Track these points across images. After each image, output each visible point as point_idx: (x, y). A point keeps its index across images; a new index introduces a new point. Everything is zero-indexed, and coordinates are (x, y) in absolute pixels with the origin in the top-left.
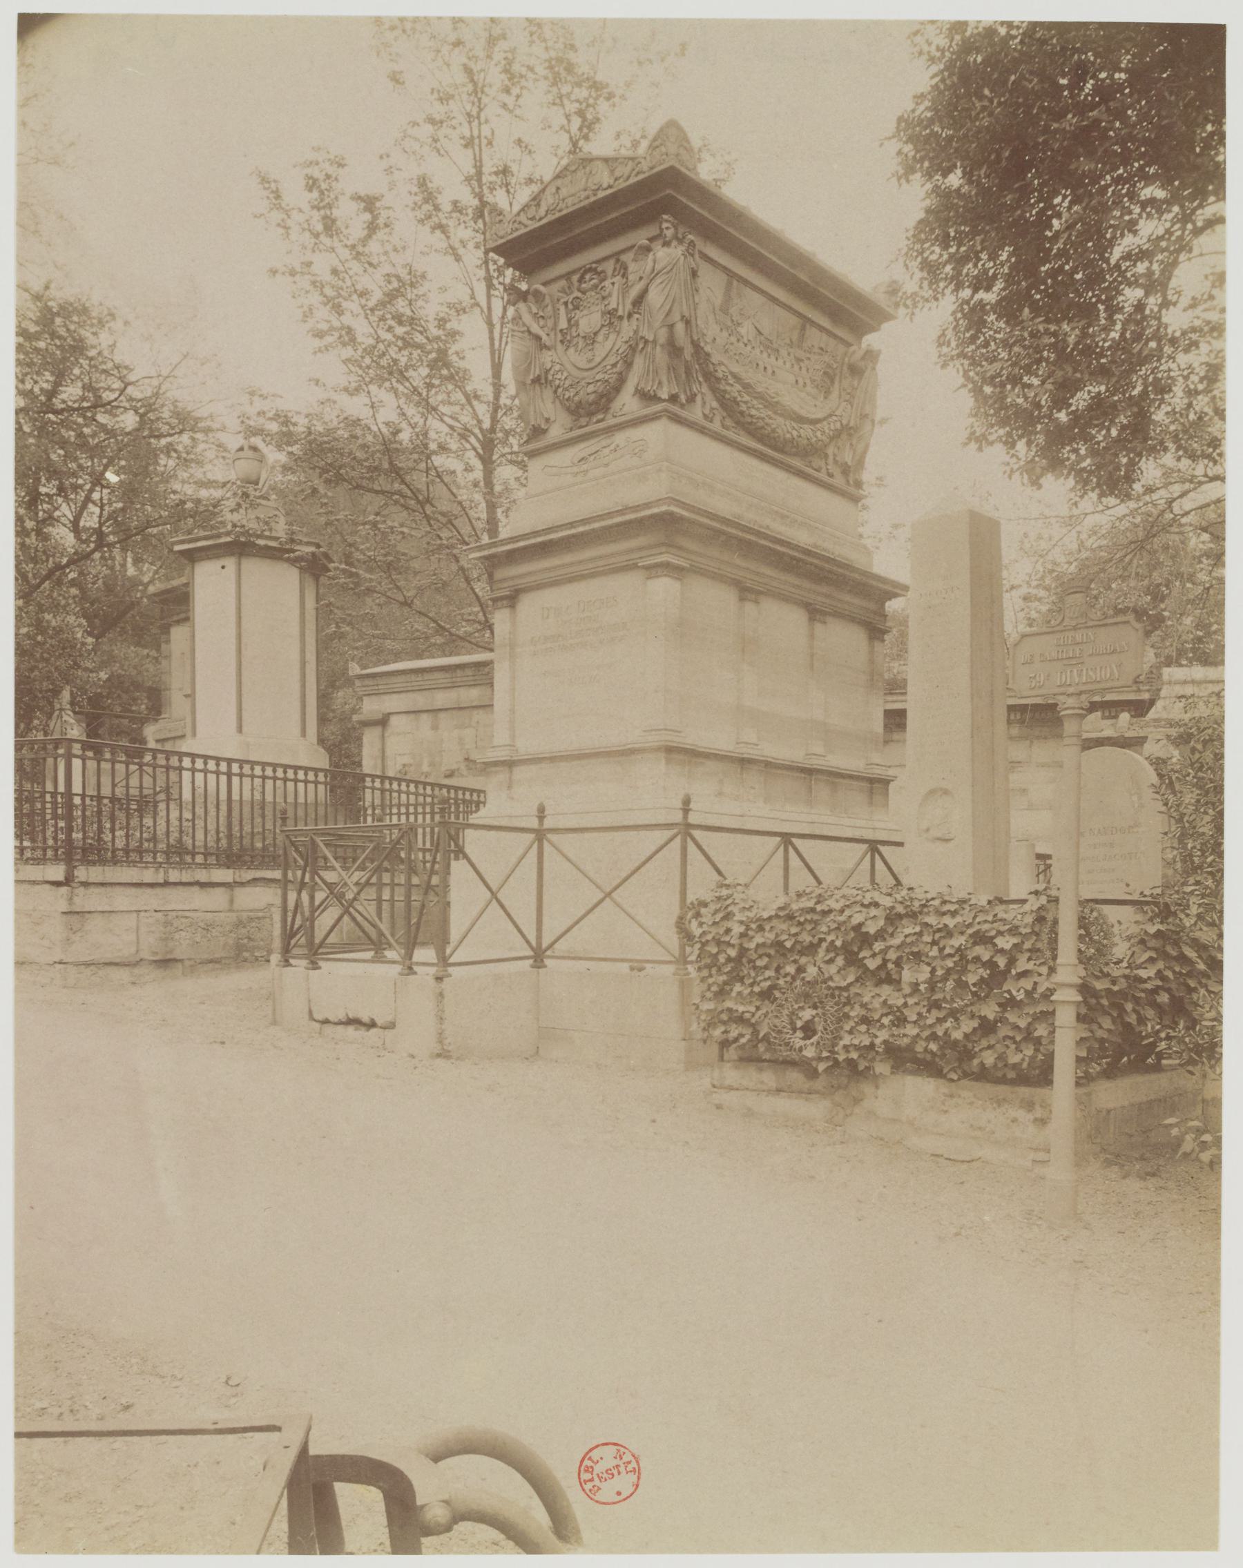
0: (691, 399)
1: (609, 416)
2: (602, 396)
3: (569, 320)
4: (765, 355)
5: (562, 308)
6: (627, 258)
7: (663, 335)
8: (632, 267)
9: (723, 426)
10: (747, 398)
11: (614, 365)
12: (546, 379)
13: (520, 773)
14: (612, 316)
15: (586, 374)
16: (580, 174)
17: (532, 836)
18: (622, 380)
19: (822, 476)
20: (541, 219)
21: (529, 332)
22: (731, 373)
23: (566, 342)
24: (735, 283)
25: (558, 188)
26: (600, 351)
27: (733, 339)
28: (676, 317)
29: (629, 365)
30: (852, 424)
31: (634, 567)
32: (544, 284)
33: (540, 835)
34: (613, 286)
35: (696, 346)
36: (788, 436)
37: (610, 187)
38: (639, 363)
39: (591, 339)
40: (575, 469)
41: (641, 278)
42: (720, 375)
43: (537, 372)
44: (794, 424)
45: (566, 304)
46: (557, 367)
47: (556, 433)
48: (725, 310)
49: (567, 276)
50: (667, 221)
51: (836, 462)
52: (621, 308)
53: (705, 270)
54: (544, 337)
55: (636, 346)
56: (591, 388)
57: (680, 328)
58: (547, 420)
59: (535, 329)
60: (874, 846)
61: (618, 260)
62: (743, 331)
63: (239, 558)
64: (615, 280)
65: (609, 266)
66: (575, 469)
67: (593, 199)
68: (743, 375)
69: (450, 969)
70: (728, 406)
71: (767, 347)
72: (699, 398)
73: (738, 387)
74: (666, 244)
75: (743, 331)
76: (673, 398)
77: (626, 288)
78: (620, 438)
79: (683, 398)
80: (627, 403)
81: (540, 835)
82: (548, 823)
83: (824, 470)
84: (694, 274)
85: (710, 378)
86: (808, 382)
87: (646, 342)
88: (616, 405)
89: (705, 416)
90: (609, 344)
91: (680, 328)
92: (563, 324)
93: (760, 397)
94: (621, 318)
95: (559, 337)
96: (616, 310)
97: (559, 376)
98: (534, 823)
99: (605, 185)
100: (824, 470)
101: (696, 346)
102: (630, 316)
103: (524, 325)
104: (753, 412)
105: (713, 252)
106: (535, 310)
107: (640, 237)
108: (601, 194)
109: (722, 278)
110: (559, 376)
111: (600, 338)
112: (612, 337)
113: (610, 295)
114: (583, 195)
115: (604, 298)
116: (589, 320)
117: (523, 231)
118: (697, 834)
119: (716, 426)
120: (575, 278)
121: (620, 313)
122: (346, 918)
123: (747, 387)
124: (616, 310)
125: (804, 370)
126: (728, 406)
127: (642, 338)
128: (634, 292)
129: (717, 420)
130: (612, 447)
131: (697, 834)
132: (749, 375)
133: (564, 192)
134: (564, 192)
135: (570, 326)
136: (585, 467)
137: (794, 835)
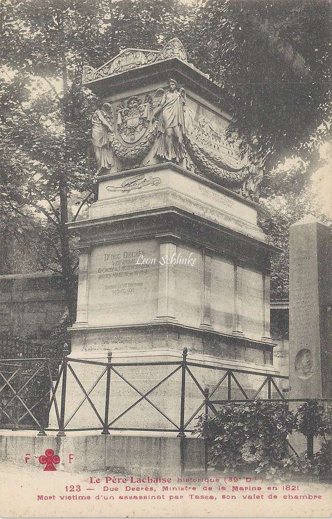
0: (181, 160)
1: (141, 166)
2: (138, 156)
3: (122, 120)
4: (215, 140)
5: (119, 114)
6: (153, 95)
7: (170, 131)
8: (155, 99)
9: (195, 172)
10: (206, 160)
11: (145, 143)
12: (110, 146)
13: (91, 337)
14: (144, 121)
15: (131, 146)
16: (131, 56)
17: (105, 367)
18: (149, 149)
19: (240, 195)
20: (110, 75)
21: (102, 123)
22: (199, 148)
23: (120, 129)
24: (201, 107)
25: (119, 61)
26: (137, 136)
27: (200, 133)
28: (176, 123)
29: (152, 143)
30: (254, 172)
31: (154, 238)
32: (111, 103)
33: (109, 367)
34: (145, 107)
35: (184, 136)
36: (225, 177)
37: (145, 64)
38: (157, 143)
39: (133, 130)
40: (123, 189)
41: (159, 105)
42: (194, 149)
43: (106, 143)
44: (227, 172)
45: (121, 113)
46: (116, 141)
47: (113, 172)
48: (196, 119)
49: (122, 100)
50: (172, 82)
51: (246, 190)
52: (149, 117)
53: (189, 102)
54: (110, 128)
55: (157, 135)
56: (133, 152)
57: (178, 129)
58: (110, 165)
59: (105, 122)
60: (230, 372)
61: (147, 96)
62: (204, 129)
63: (283, 343)
64: (145, 104)
65: (143, 98)
66: (123, 189)
67: (137, 68)
68: (205, 149)
69: (66, 433)
70: (198, 163)
71: (215, 136)
72: (184, 160)
73: (203, 155)
74: (172, 91)
75: (204, 129)
76: (174, 160)
77: (152, 108)
78: (147, 176)
79: (178, 160)
80: (151, 161)
81: (109, 367)
82: (113, 361)
83: (241, 193)
84: (184, 104)
85: (190, 151)
86: (234, 152)
87: (161, 133)
88: (146, 160)
89: (187, 168)
90: (142, 133)
91: (178, 129)
92: (120, 122)
93: (212, 159)
95: (117, 127)
96: (146, 118)
97: (117, 145)
98: (106, 361)
99: (143, 63)
100: (241, 193)
101: (184, 136)
102: (153, 121)
103: (100, 120)
104: (209, 166)
105: (192, 94)
106: (105, 114)
107: (160, 87)
108: (141, 67)
109: (195, 105)
110: (117, 145)
111: (138, 129)
112: (144, 130)
113: (143, 111)
114: (132, 66)
115: (140, 112)
116: (133, 121)
117: (101, 78)
118: (189, 367)
119: (192, 172)
120: (126, 101)
121: (148, 119)
122: (245, 399)
123: (207, 155)
124: (146, 118)
125: (232, 147)
126: (198, 163)
127: (159, 131)
128: (155, 111)
129: (193, 169)
130: (143, 180)
131: (189, 367)
132: (208, 150)
133: (123, 63)
134: (123, 63)
135: (123, 123)
136: (128, 188)
137: (233, 370)
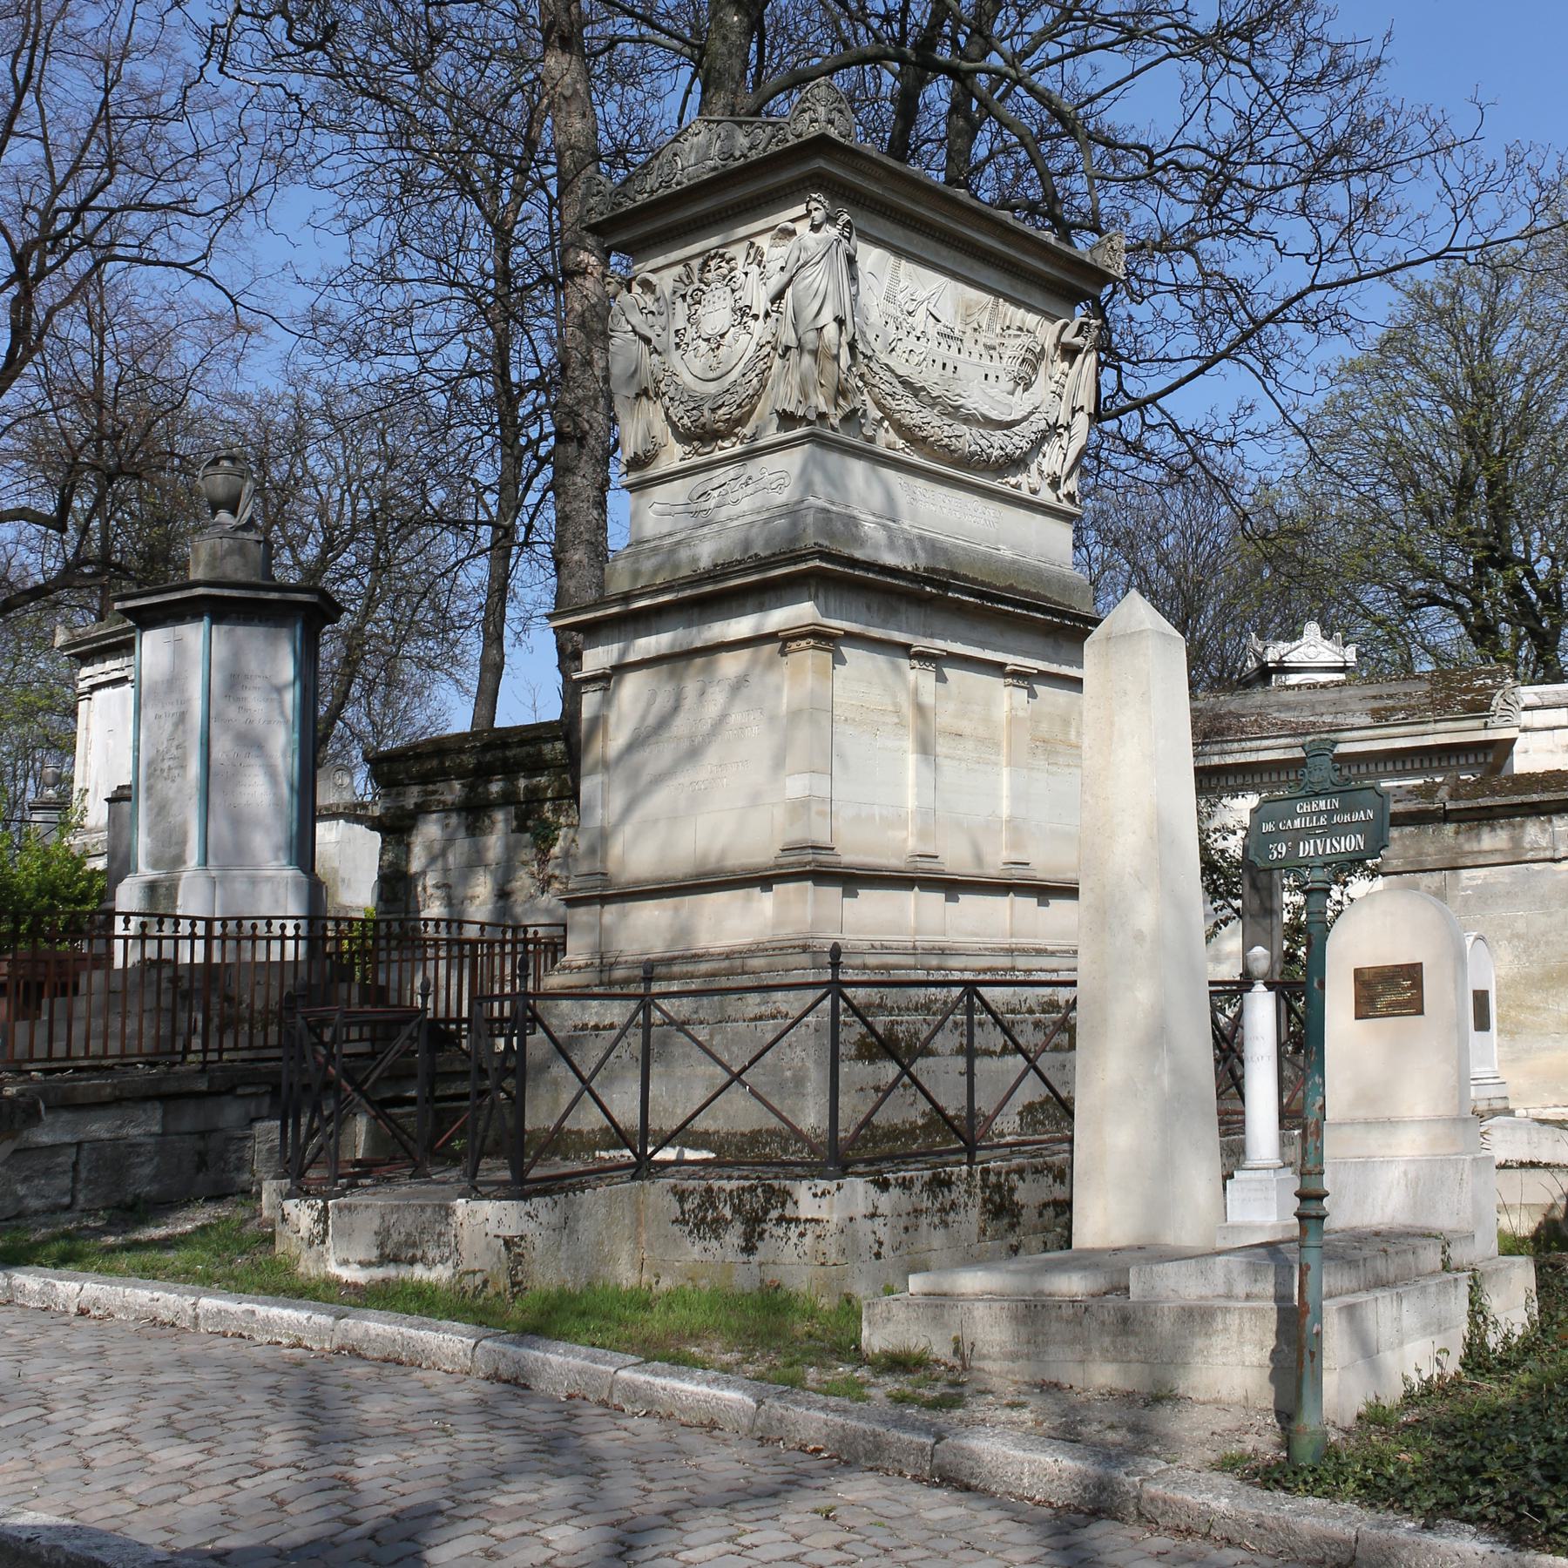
92: (680, 323)
94: (756, 317)
